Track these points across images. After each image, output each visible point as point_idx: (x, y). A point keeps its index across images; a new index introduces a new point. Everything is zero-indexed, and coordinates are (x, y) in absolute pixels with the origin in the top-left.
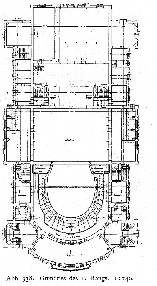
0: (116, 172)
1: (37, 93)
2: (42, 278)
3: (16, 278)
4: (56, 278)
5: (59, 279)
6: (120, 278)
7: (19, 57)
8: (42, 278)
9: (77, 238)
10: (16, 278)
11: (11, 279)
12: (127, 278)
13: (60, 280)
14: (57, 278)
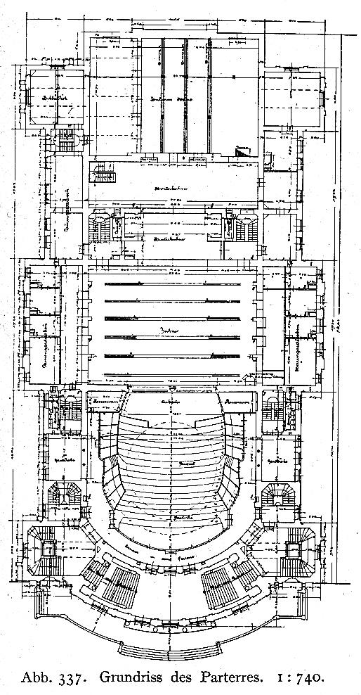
0: (271, 411)
1: (97, 233)
2: (106, 677)
3: (43, 678)
4: (138, 678)
5: (146, 678)
6: (289, 676)
7: (58, 150)
8: (106, 677)
9: (185, 563)
10: (43, 678)
11: (32, 679)
12: (309, 675)
13: (148, 681)
14: (141, 678)
